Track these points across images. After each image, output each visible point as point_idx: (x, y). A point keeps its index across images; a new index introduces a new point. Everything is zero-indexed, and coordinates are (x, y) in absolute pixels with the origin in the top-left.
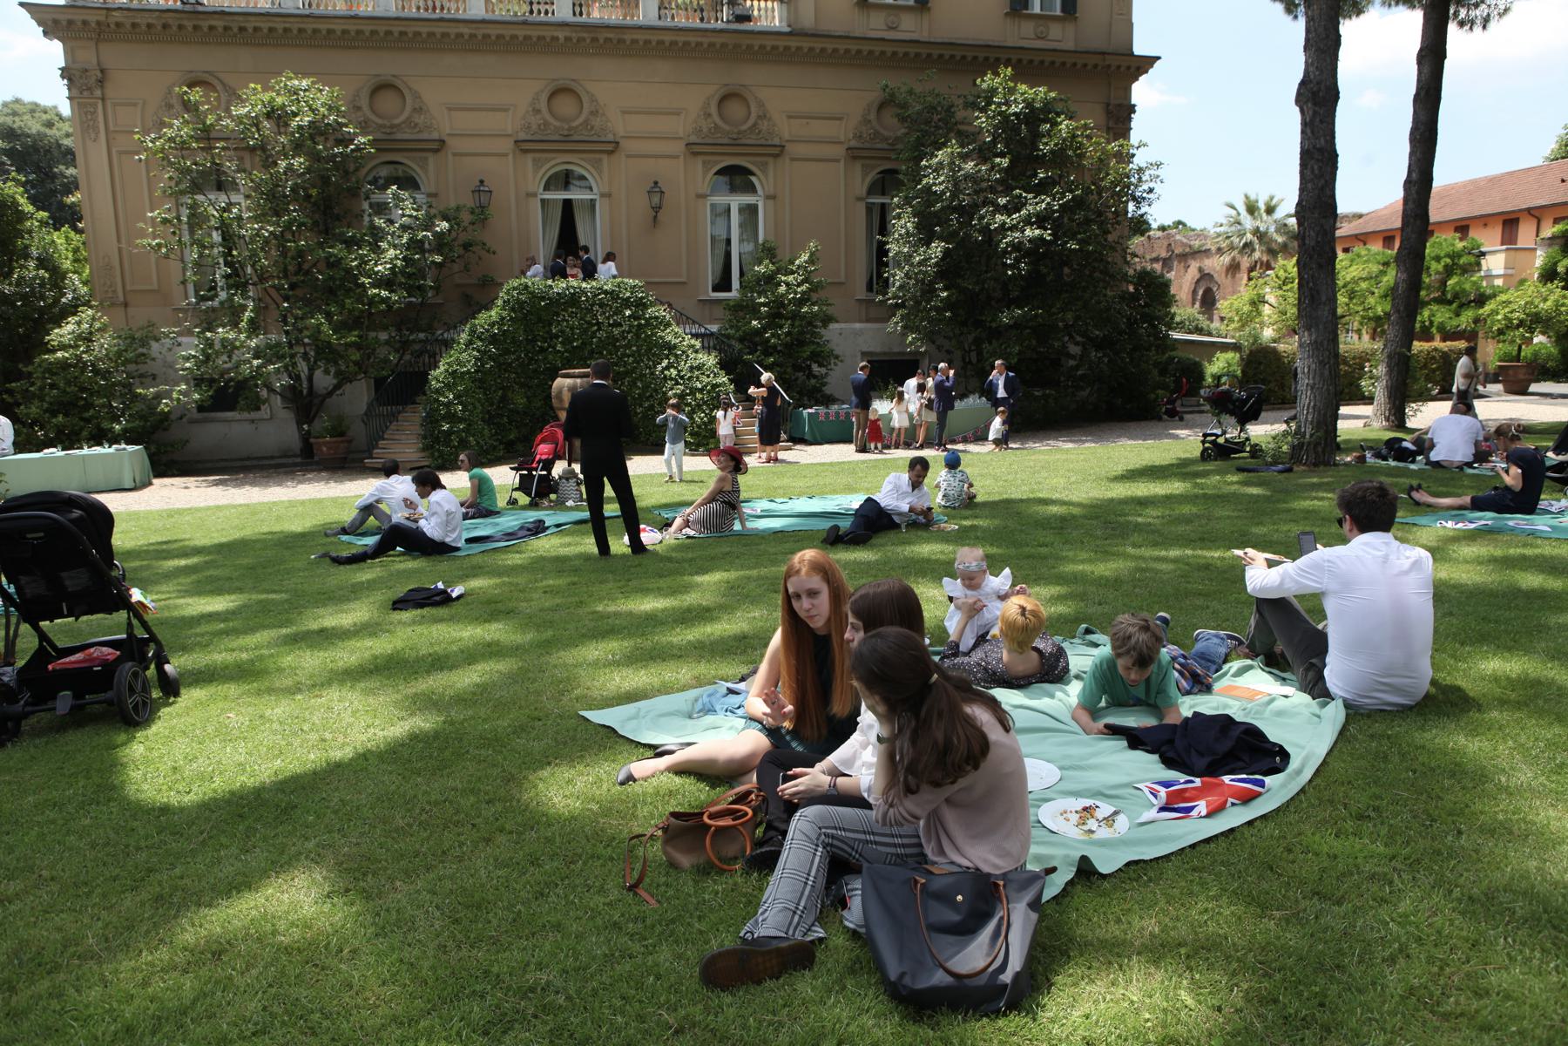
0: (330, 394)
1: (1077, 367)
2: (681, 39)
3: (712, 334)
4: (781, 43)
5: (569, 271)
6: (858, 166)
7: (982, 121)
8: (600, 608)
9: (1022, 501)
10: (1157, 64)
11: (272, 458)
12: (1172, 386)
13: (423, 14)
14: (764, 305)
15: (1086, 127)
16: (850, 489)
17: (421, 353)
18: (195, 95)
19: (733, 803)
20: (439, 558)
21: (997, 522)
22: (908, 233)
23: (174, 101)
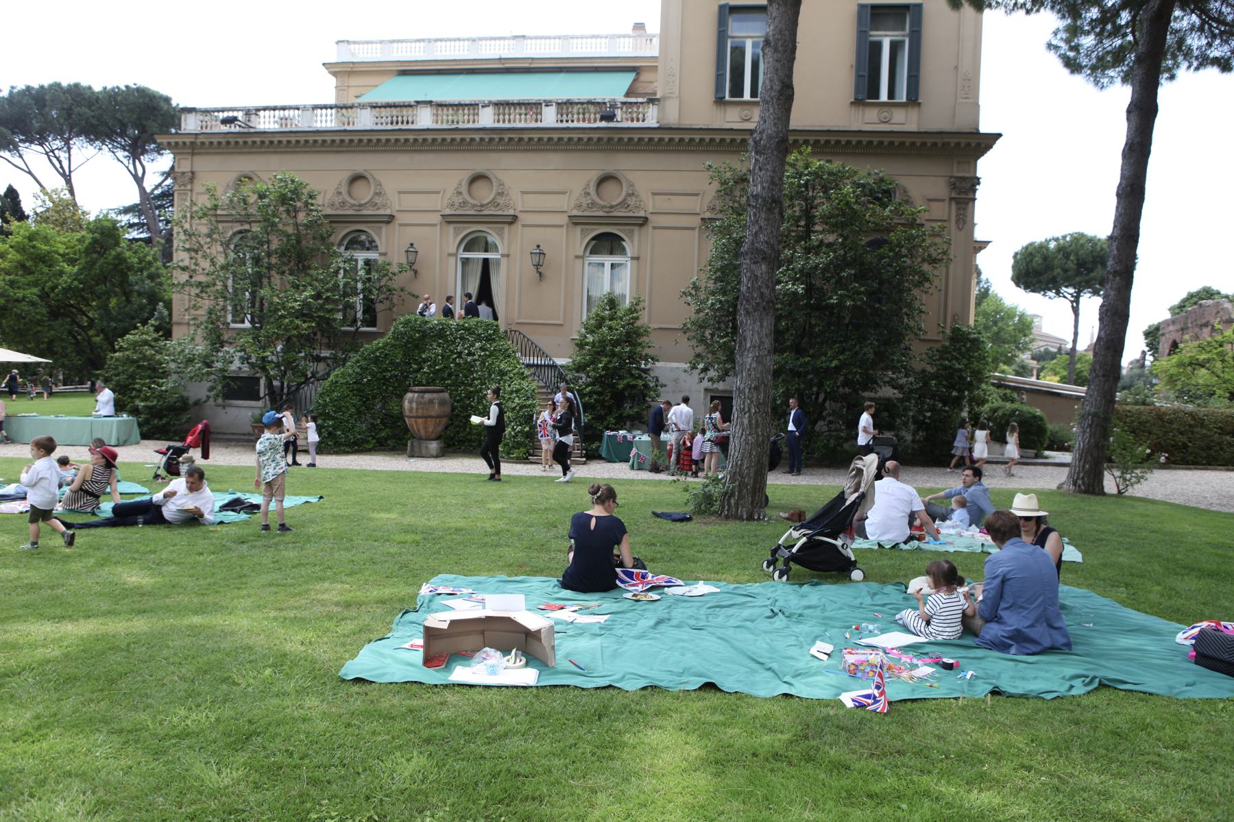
10: (999, 142)
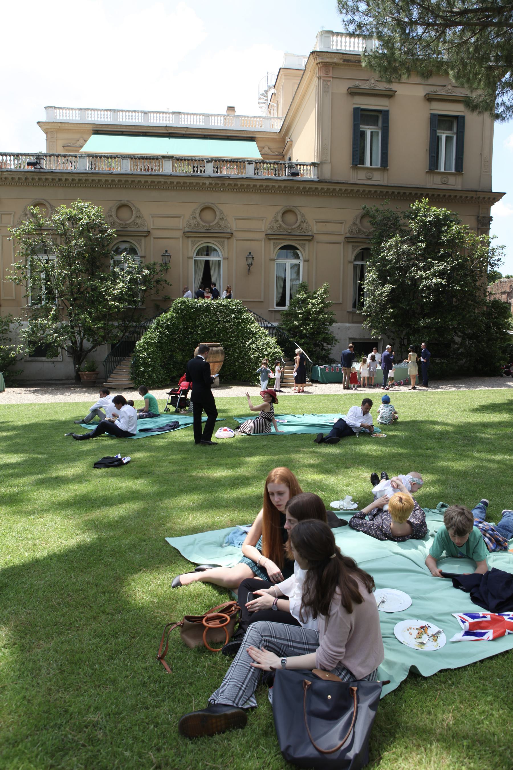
0: (90, 351)
1: (458, 349)
2: (265, 184)
3: (274, 327)
4: (314, 186)
5: (206, 295)
6: (350, 246)
7: (412, 225)
8: (194, 474)
9: (422, 422)
10: (504, 197)
11: (62, 380)
12: (509, 359)
13: (143, 172)
14: (301, 314)
15: (465, 228)
16: (335, 411)
17: (133, 333)
18: (37, 210)
19: (220, 612)
20: (124, 439)
21: (407, 433)
22: (373, 280)
23: (28, 213)
